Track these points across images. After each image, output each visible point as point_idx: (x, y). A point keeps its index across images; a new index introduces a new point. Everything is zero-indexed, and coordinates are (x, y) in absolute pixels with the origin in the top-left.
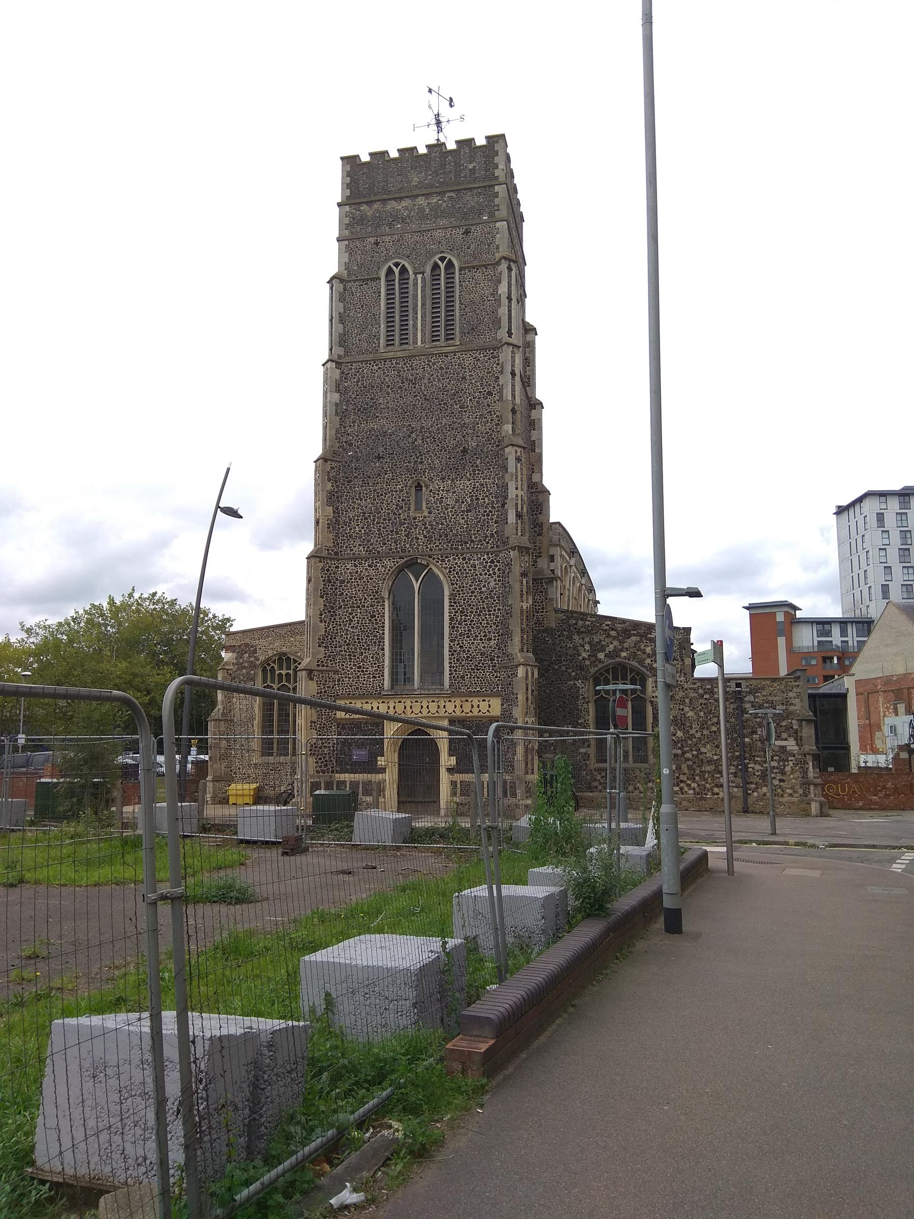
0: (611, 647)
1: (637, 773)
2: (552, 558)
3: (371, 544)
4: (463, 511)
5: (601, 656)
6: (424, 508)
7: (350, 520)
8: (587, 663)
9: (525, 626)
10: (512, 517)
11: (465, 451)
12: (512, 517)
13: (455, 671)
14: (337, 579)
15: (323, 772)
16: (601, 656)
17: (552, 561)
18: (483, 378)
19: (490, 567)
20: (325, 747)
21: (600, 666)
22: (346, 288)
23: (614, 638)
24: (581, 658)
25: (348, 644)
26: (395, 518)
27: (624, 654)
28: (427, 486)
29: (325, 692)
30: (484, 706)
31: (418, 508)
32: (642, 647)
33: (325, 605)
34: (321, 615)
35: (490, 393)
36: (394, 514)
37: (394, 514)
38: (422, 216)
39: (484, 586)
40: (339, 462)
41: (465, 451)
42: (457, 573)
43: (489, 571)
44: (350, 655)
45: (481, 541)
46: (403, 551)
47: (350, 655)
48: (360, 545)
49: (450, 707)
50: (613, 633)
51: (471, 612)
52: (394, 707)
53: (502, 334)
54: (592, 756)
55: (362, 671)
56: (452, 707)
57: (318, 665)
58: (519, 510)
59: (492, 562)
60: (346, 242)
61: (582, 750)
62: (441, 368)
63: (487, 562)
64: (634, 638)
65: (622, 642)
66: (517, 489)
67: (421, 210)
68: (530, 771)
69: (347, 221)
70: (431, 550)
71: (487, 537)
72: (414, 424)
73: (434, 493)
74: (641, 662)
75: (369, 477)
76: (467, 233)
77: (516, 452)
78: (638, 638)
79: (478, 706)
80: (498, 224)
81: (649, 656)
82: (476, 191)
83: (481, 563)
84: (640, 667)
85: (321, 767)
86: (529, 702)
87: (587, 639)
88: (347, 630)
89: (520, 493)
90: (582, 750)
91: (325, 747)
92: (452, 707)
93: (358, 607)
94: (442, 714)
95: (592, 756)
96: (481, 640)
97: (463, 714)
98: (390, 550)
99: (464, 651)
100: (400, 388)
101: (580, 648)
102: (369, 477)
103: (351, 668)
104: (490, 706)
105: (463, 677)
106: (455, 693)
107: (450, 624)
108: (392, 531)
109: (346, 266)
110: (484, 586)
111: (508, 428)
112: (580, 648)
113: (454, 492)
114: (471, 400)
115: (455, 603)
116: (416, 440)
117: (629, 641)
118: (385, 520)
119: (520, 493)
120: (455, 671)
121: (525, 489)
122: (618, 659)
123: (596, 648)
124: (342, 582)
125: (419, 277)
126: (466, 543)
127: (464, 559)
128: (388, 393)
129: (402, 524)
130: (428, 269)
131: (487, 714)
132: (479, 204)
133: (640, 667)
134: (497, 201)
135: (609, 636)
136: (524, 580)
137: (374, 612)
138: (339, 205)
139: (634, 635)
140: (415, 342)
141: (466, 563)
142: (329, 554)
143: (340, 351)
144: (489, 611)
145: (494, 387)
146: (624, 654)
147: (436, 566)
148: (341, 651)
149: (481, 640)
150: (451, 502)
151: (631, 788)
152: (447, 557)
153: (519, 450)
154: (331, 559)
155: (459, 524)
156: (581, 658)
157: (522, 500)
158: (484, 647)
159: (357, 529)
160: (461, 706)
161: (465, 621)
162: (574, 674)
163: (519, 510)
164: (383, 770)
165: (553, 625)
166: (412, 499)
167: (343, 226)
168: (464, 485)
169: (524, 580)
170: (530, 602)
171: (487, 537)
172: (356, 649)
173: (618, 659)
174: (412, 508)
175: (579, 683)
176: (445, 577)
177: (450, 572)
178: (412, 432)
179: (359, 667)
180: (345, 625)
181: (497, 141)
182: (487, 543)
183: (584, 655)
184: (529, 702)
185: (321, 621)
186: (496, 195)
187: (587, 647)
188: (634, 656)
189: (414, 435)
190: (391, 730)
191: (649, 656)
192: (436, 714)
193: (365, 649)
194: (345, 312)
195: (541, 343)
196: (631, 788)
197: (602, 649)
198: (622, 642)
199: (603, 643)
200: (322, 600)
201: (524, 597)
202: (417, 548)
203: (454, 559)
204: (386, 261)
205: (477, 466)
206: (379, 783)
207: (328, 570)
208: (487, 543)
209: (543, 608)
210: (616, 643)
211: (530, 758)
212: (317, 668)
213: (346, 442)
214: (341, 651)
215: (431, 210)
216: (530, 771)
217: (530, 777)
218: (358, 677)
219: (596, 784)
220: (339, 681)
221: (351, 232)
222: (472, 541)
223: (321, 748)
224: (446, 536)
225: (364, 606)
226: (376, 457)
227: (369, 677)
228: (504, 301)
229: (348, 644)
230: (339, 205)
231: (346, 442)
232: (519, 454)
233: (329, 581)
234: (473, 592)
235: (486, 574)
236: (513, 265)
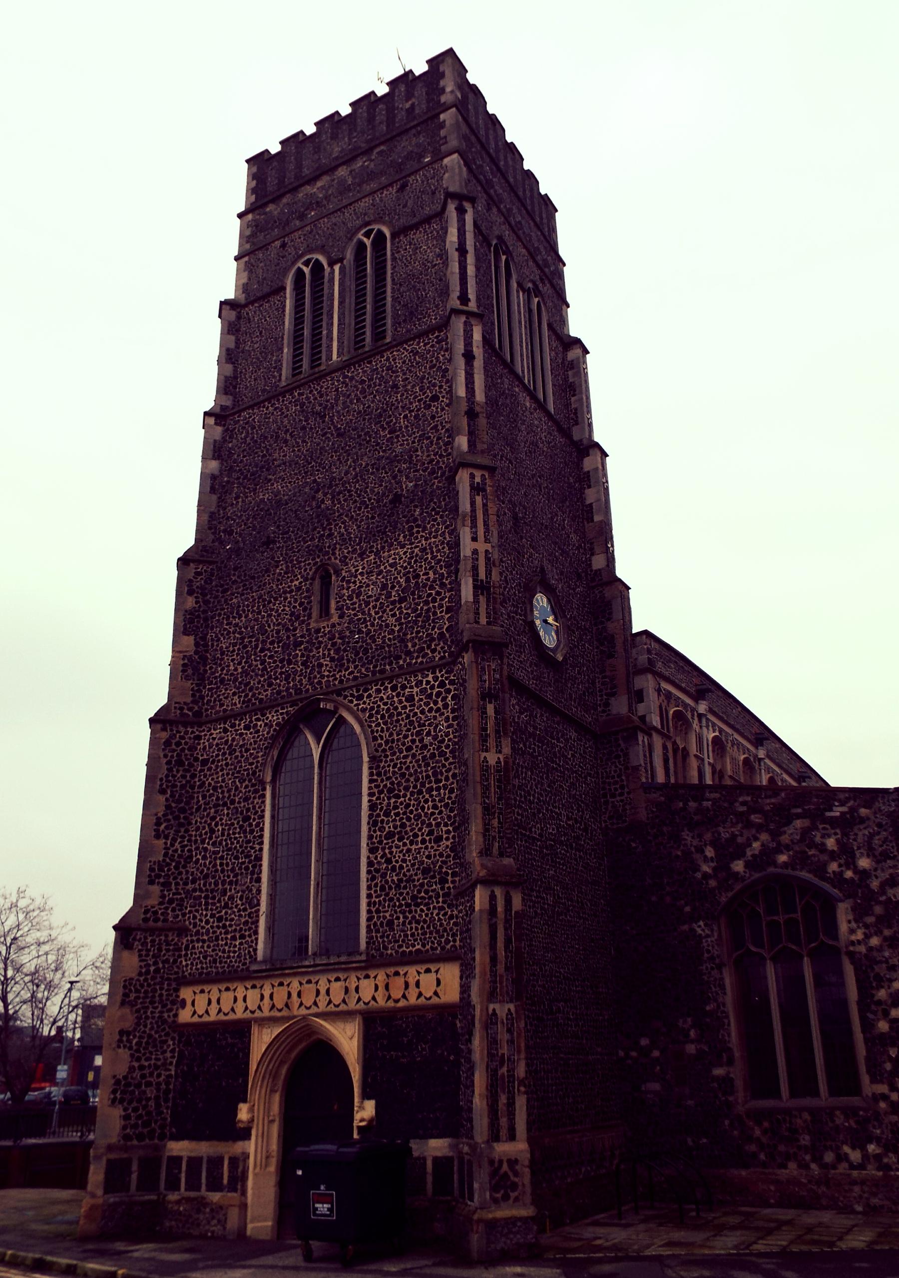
0: (756, 845)
1: (840, 1119)
2: (639, 696)
3: (251, 689)
4: (393, 603)
5: (738, 866)
6: (333, 611)
7: (222, 653)
8: (713, 883)
9: (493, 799)
10: (467, 592)
11: (397, 499)
12: (467, 592)
13: (378, 911)
14: (196, 759)
15: (140, 1137)
16: (738, 866)
17: (641, 699)
18: (423, 377)
19: (439, 694)
20: (148, 1084)
21: (738, 887)
22: (238, 317)
23: (760, 828)
24: (699, 875)
25: (206, 877)
26: (288, 637)
27: (783, 858)
28: (338, 572)
29: (157, 971)
30: (428, 982)
31: (325, 612)
32: (818, 839)
33: (168, 807)
34: (158, 824)
35: (435, 398)
36: (288, 630)
37: (288, 630)
38: (344, 189)
39: (429, 734)
40: (211, 563)
41: (397, 499)
42: (383, 717)
43: (436, 703)
44: (206, 897)
45: (422, 649)
46: (298, 691)
47: (206, 897)
48: (234, 694)
49: (367, 989)
50: (756, 818)
51: (407, 788)
52: (328, 992)
53: (454, 302)
54: (739, 1083)
55: (224, 926)
56: (369, 990)
57: (145, 920)
58: (482, 575)
59: (443, 684)
60: (246, 259)
61: (718, 1072)
62: (363, 382)
63: (432, 687)
64: (798, 823)
65: (775, 835)
66: (474, 539)
67: (342, 181)
68: (503, 1133)
69: (248, 232)
70: (341, 682)
71: (433, 639)
72: (319, 477)
73: (349, 582)
74: (820, 870)
75: (253, 578)
76: (402, 189)
77: (472, 476)
78: (806, 823)
79: (418, 984)
80: (446, 161)
81: (833, 856)
82: (414, 131)
83: (424, 691)
84: (816, 881)
85: (135, 1126)
86: (501, 968)
87: (708, 836)
88: (206, 849)
89: (482, 546)
90: (718, 1072)
91: (148, 1084)
92: (369, 990)
93: (225, 804)
94: (352, 1005)
95: (739, 1083)
96: (423, 841)
97: (391, 1004)
98: (279, 693)
99: (393, 869)
100: (303, 428)
101: (697, 856)
102: (253, 578)
103: (207, 922)
104: (439, 982)
105: (390, 923)
106: (374, 960)
107: (370, 816)
108: (282, 661)
109: (244, 288)
110: (429, 734)
111: (462, 442)
112: (697, 856)
113: (381, 572)
114: (405, 417)
115: (379, 774)
116: (323, 501)
117: (790, 830)
118: (272, 643)
119: (482, 546)
120: (378, 911)
121: (495, 539)
122: (771, 869)
123: (729, 850)
124: (205, 762)
125: (337, 268)
126: (398, 658)
127: (394, 688)
128: (286, 441)
129: (297, 644)
130: (349, 255)
131: (435, 1000)
132: (418, 145)
133: (816, 881)
134: (443, 133)
135: (749, 825)
136: (490, 709)
137: (248, 810)
138: (240, 216)
139: (798, 816)
140: (329, 358)
141: (398, 695)
142: (182, 715)
143: (228, 401)
144: (438, 781)
145: (441, 387)
146: (783, 858)
147: (349, 709)
148: (195, 890)
149: (423, 841)
150: (373, 591)
151: (829, 1157)
152: (366, 690)
153: (478, 474)
154: (185, 725)
155: (387, 626)
156: (699, 875)
157: (487, 559)
158: (429, 857)
159: (232, 668)
160: (387, 987)
161: (395, 807)
162: (688, 909)
163: (482, 575)
164: (245, 1134)
165: (643, 815)
166: (315, 599)
167: (244, 238)
168: (399, 554)
169: (490, 709)
170: (507, 750)
171: (433, 639)
172: (216, 884)
173: (771, 869)
174: (315, 613)
175: (700, 928)
176: (362, 726)
177: (371, 716)
178: (317, 491)
179: (220, 919)
180: (203, 842)
181: (446, 63)
182: (434, 651)
183: (706, 868)
184: (501, 968)
185: (157, 837)
186: (442, 125)
187: (710, 852)
188: (799, 860)
189: (320, 495)
190: (261, 1041)
191: (833, 856)
192: (343, 1007)
193: (231, 883)
194: (237, 347)
195: (597, 370)
196: (829, 1157)
197: (739, 853)
198: (775, 835)
199: (740, 840)
200: (162, 799)
201: (491, 742)
202: (320, 683)
203: (378, 691)
204: (294, 263)
205: (416, 520)
206: (234, 1161)
207: (178, 744)
208: (434, 651)
209: (622, 787)
210: (764, 837)
211: (503, 1099)
212: (143, 925)
213: (225, 531)
214: (195, 890)
215: (354, 178)
216: (503, 1133)
217: (503, 1148)
218: (217, 939)
219: (753, 1148)
220: (187, 948)
221: (253, 244)
222: (408, 653)
223: (138, 1086)
224: (366, 651)
225: (233, 802)
226: (264, 544)
227: (234, 938)
228: (454, 256)
229: (206, 877)
230: (240, 216)
231: (225, 531)
232: (478, 479)
233: (180, 763)
234: (409, 749)
235: (431, 710)
236: (467, 206)
